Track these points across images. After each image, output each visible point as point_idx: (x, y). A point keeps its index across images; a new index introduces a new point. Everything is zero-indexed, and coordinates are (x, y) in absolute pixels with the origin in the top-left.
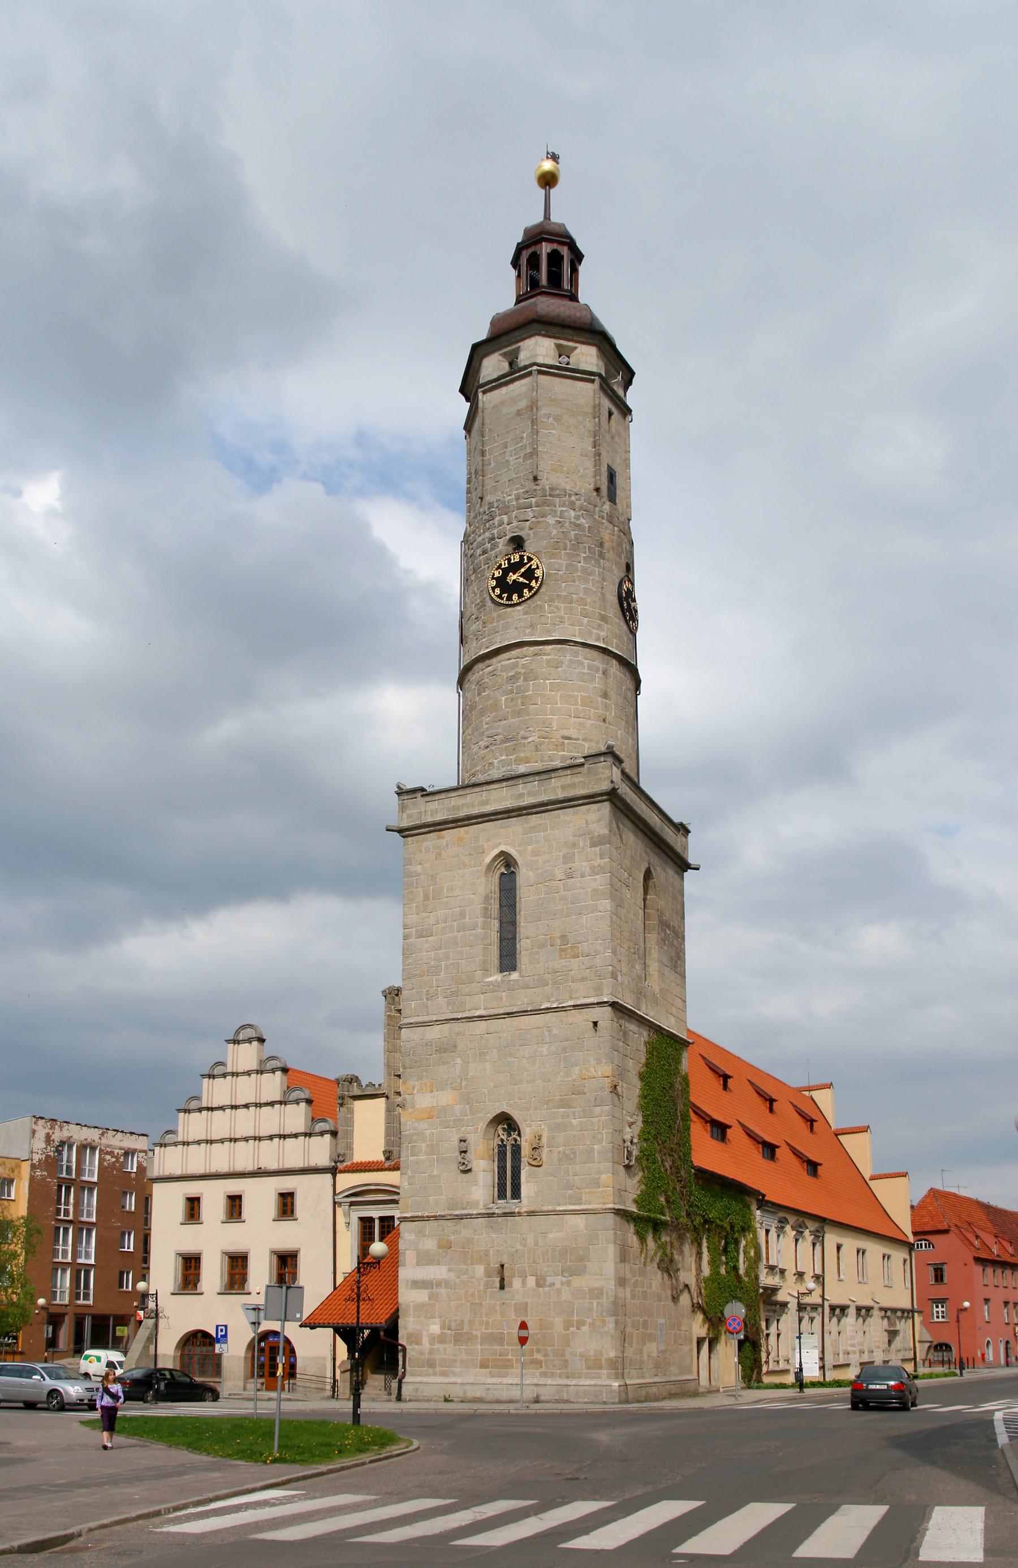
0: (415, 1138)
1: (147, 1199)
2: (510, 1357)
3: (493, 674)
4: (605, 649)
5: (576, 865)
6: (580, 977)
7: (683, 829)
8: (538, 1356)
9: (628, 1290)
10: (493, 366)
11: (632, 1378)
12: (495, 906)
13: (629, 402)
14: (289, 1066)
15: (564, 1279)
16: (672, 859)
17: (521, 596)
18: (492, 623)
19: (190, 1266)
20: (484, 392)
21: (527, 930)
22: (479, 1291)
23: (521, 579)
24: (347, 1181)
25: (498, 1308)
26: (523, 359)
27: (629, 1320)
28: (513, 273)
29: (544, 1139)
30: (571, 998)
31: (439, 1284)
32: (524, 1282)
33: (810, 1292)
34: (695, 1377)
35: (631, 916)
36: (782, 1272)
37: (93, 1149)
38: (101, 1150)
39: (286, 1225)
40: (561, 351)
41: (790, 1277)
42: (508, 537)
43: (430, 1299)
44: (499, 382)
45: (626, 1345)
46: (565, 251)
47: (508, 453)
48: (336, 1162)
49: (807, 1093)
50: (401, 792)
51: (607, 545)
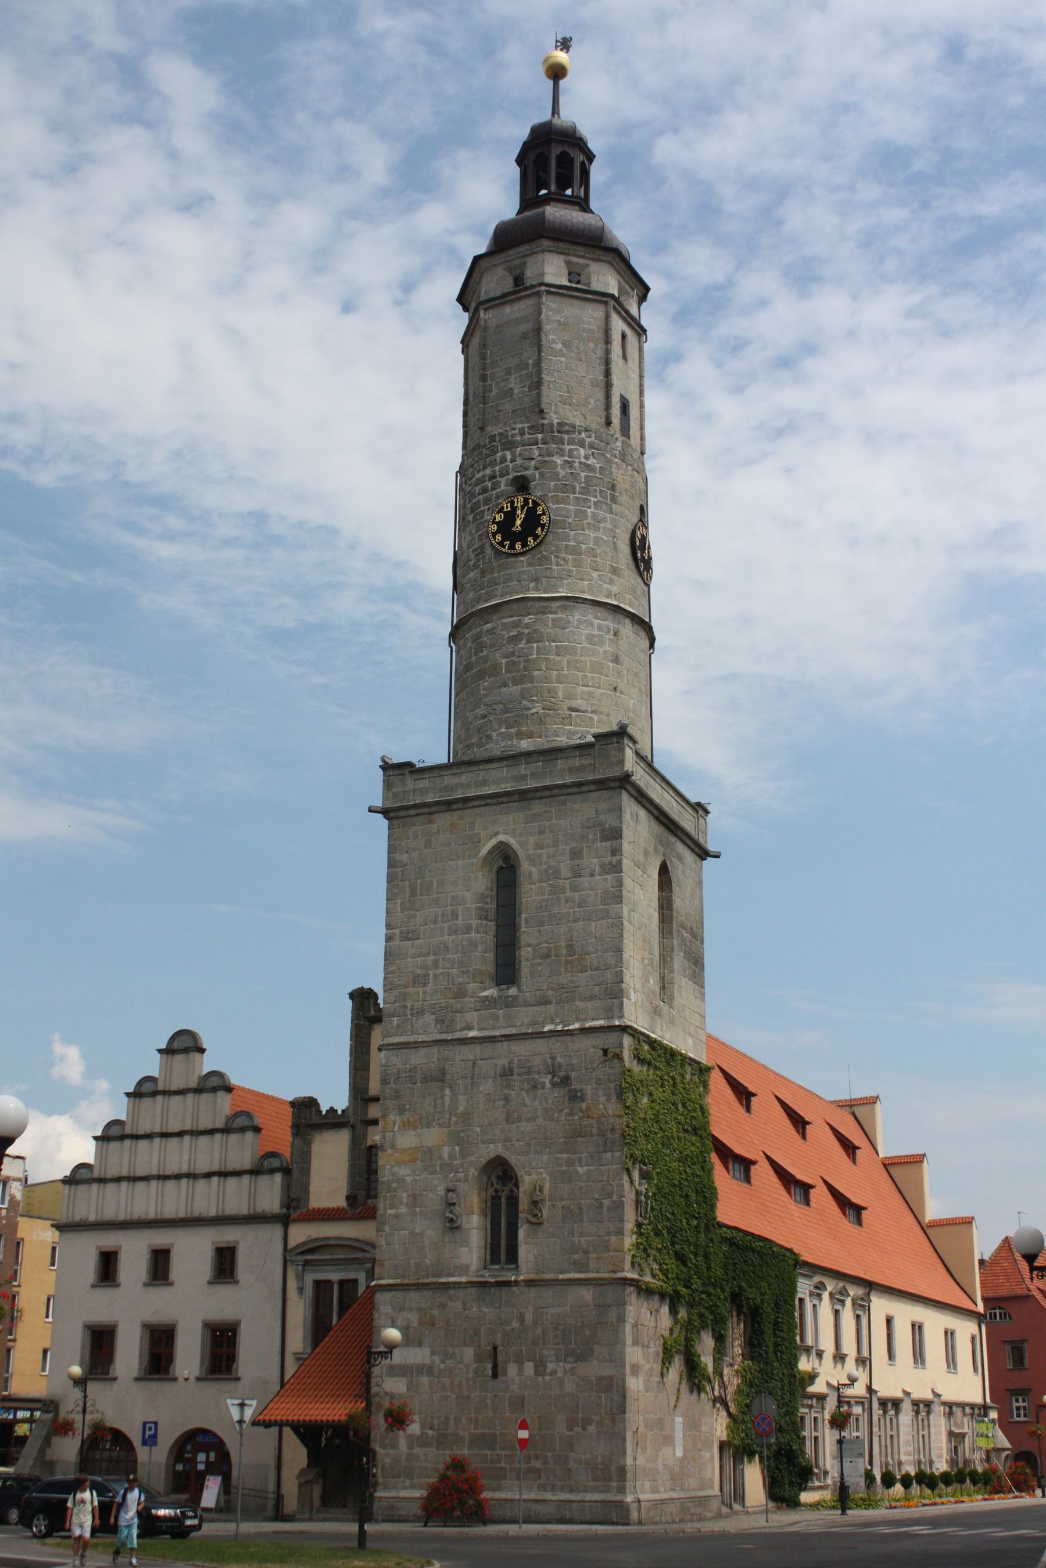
1: (18, 1244)
2: (503, 1465)
3: (491, 631)
4: (618, 607)
7: (700, 809)
8: (537, 1464)
9: (641, 1379)
13: (643, 323)
15: (568, 1366)
16: (689, 847)
17: (525, 544)
18: (492, 573)
20: (485, 310)
24: (300, 1234)
25: (488, 1401)
29: (546, 1191)
30: (578, 1020)
32: (521, 1369)
33: (853, 1380)
42: (510, 477)
43: (408, 1389)
48: (288, 1209)
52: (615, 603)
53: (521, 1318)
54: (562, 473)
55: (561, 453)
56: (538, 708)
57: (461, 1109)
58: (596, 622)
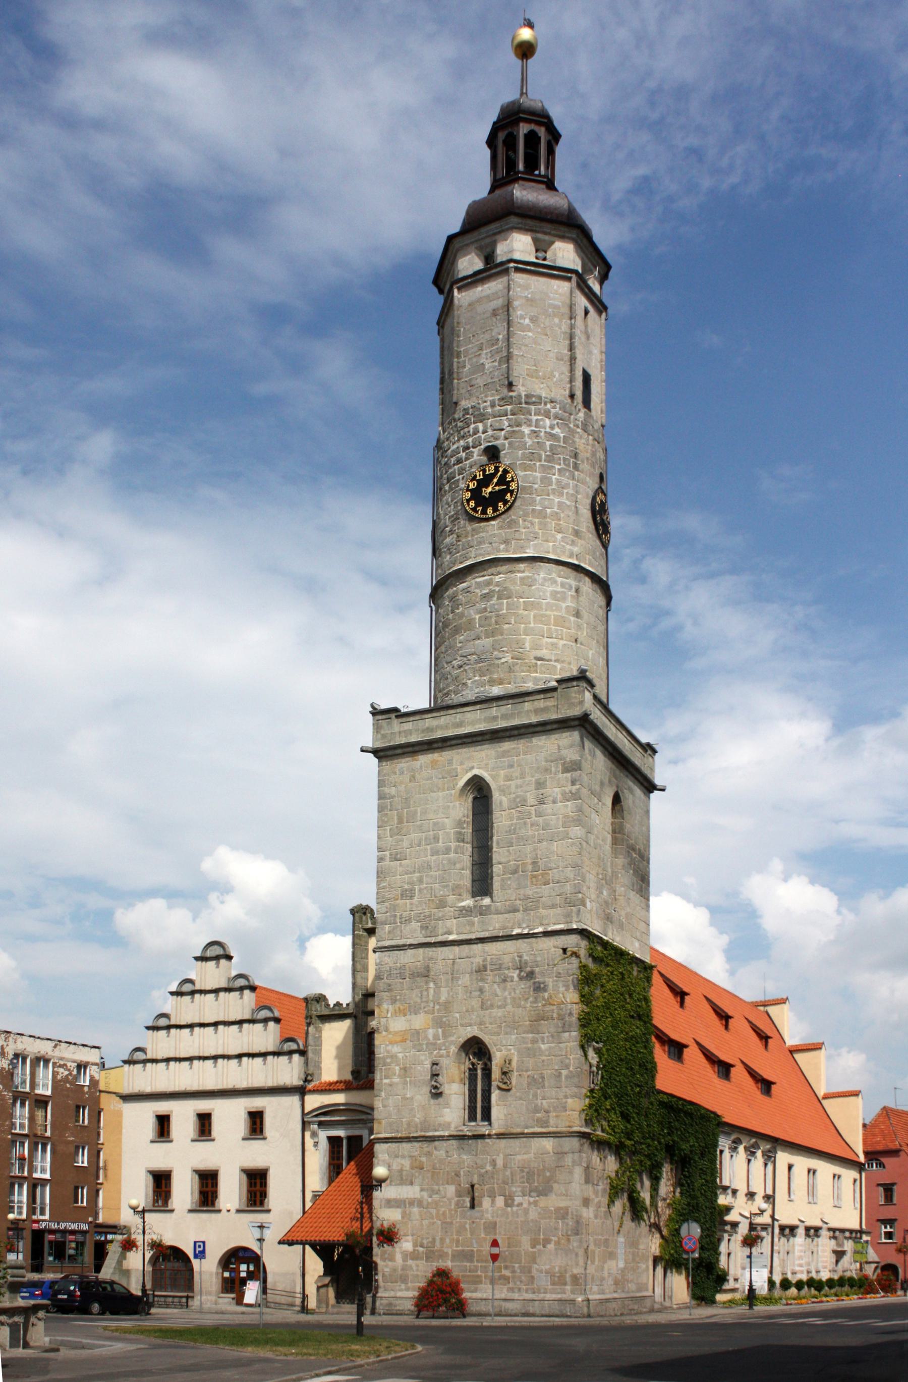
0: (388, 1060)
2: (479, 1273)
3: (467, 591)
5: (547, 791)
6: (550, 903)
8: (507, 1273)
10: (469, 263)
11: (594, 1293)
12: (468, 830)
14: (257, 983)
15: (532, 1199)
19: (161, 1181)
21: (499, 854)
22: (450, 1210)
23: (497, 488)
24: (314, 1101)
25: (467, 1226)
26: (502, 251)
27: (591, 1239)
28: (487, 152)
30: (542, 924)
31: (412, 1203)
32: (493, 1202)
33: (762, 1212)
34: (650, 1293)
35: (600, 841)
36: (735, 1192)
37: (47, 1061)
38: (54, 1064)
39: (256, 1144)
40: (541, 247)
41: (741, 1195)
42: (482, 447)
43: (403, 1217)
44: (477, 278)
45: (589, 1262)
46: (542, 132)
47: (484, 356)
49: (762, 1008)
50: (376, 712)
51: (582, 455)
52: (576, 562)
53: (494, 1163)
54: (529, 442)
55: (529, 423)
56: (507, 658)
57: (443, 999)
58: (559, 580)
